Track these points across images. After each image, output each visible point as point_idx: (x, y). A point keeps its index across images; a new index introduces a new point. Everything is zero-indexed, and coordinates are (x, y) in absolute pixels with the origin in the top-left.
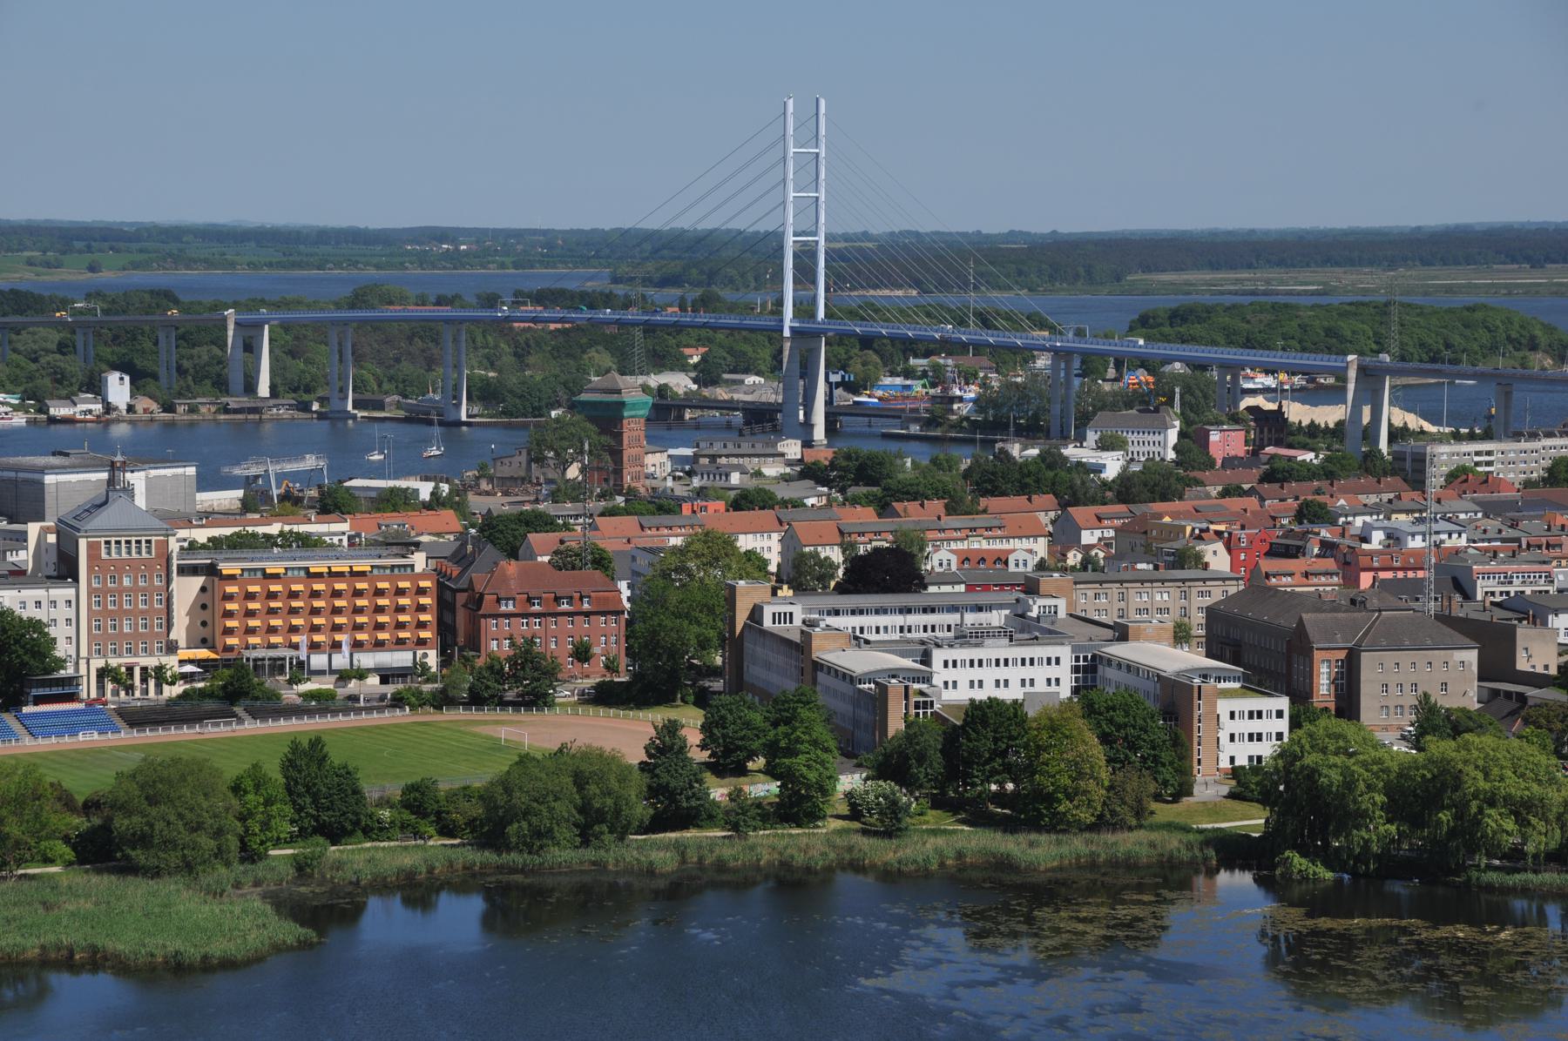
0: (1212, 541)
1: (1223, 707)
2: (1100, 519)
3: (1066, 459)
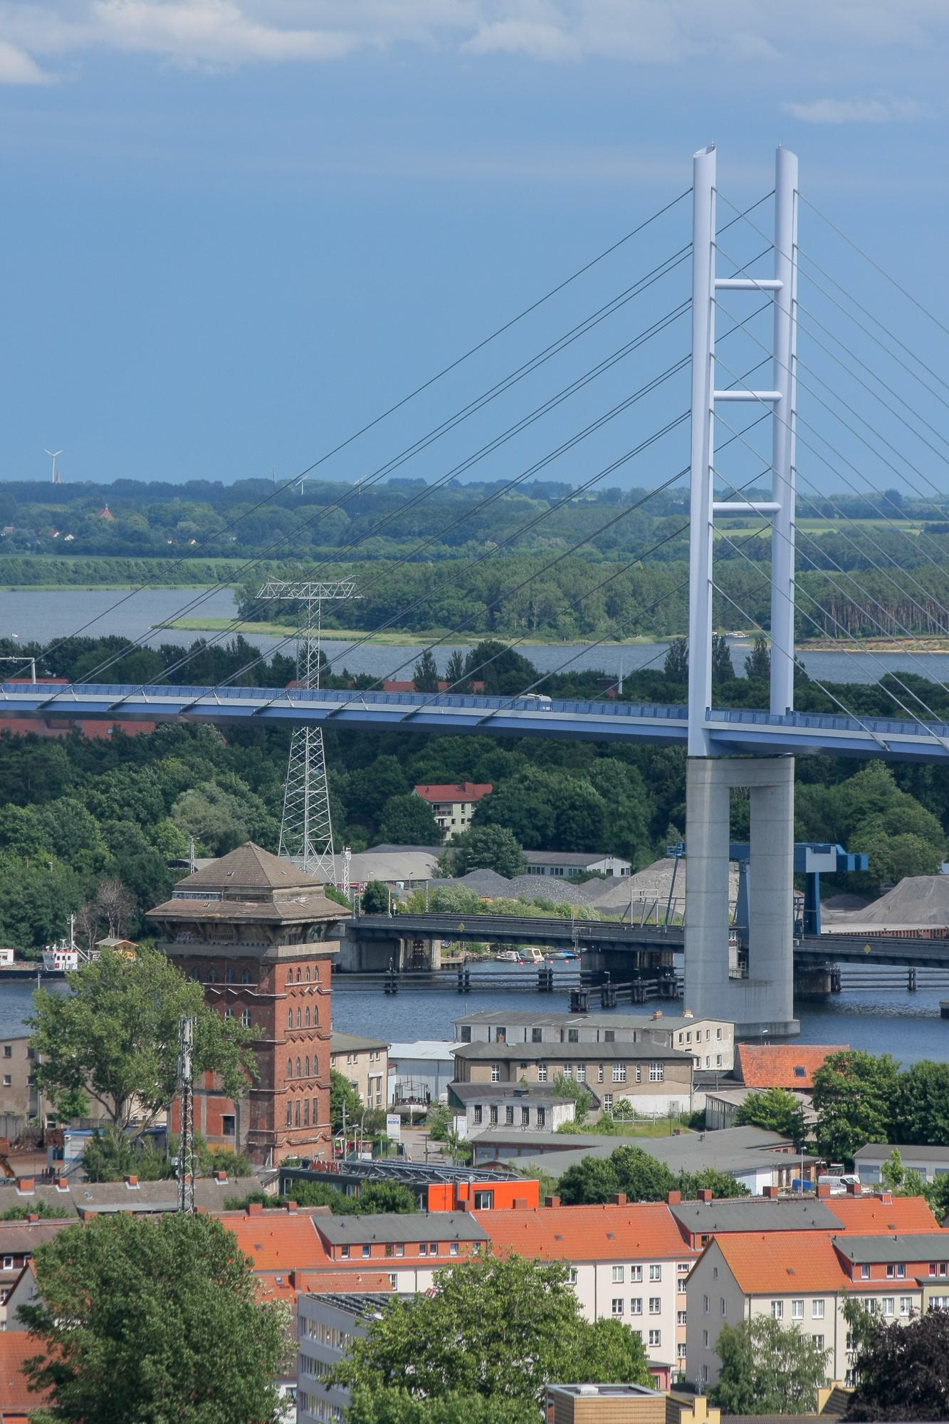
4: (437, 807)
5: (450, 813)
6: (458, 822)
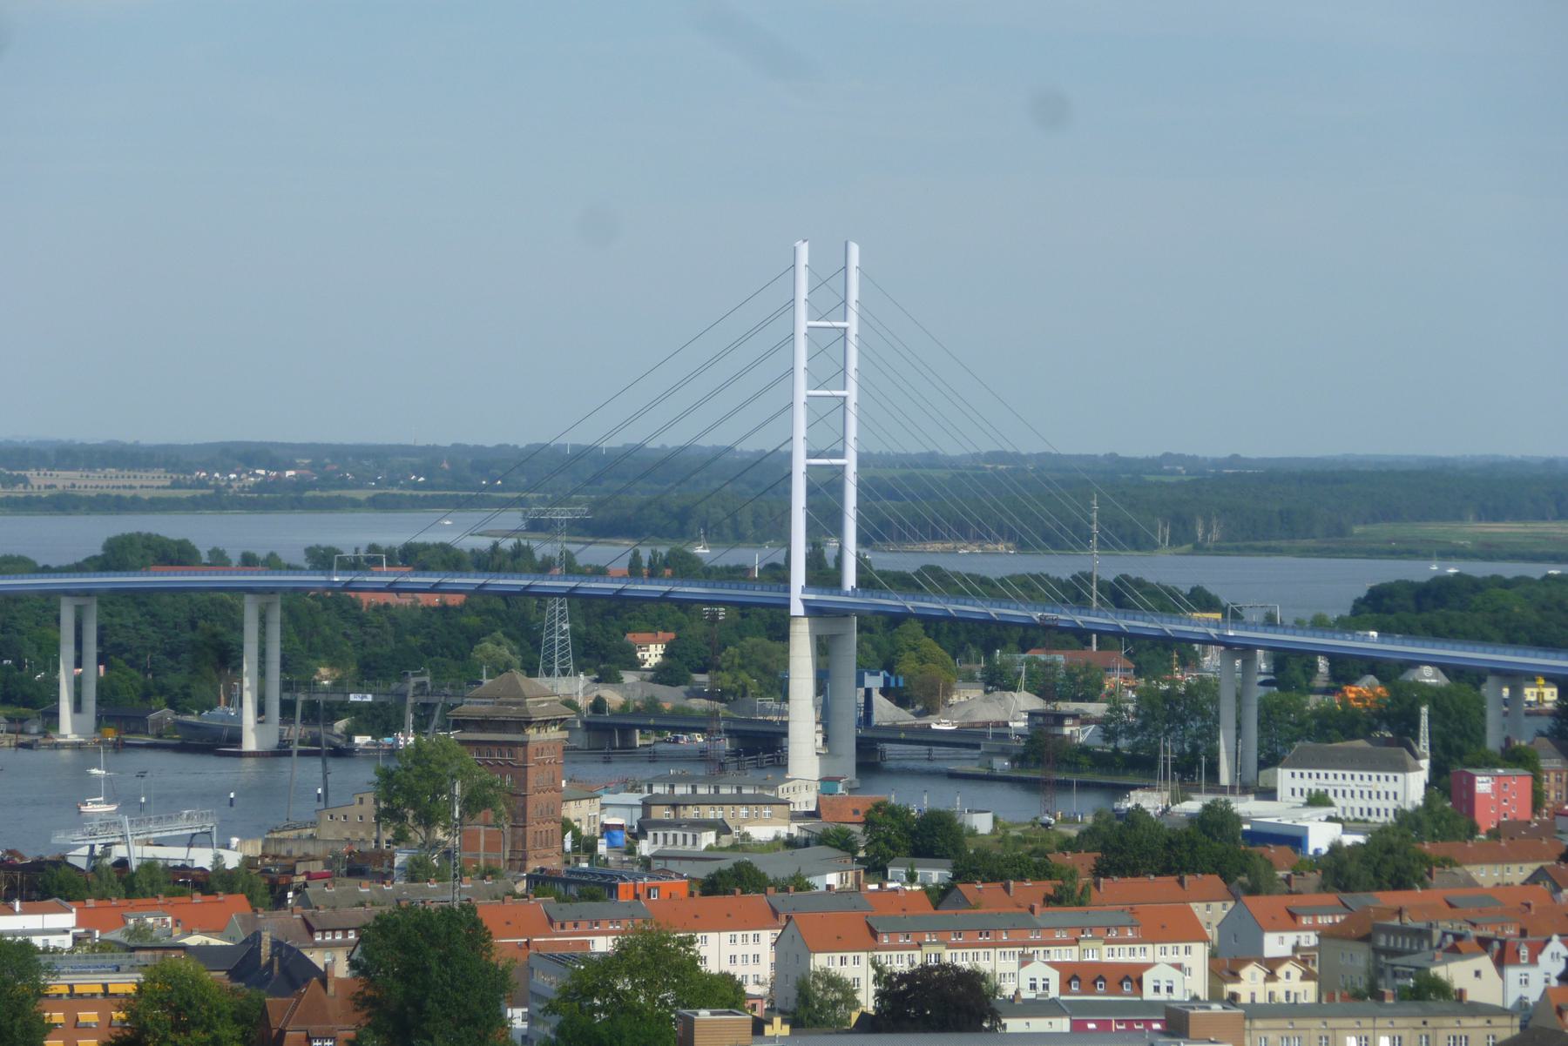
0: (1472, 954)
2: (1294, 916)
3: (1239, 820)
4: (640, 647)
5: (648, 650)
6: (653, 655)
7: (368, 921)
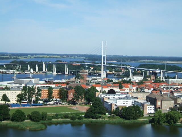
1: (148, 106)
7: (29, 114)
